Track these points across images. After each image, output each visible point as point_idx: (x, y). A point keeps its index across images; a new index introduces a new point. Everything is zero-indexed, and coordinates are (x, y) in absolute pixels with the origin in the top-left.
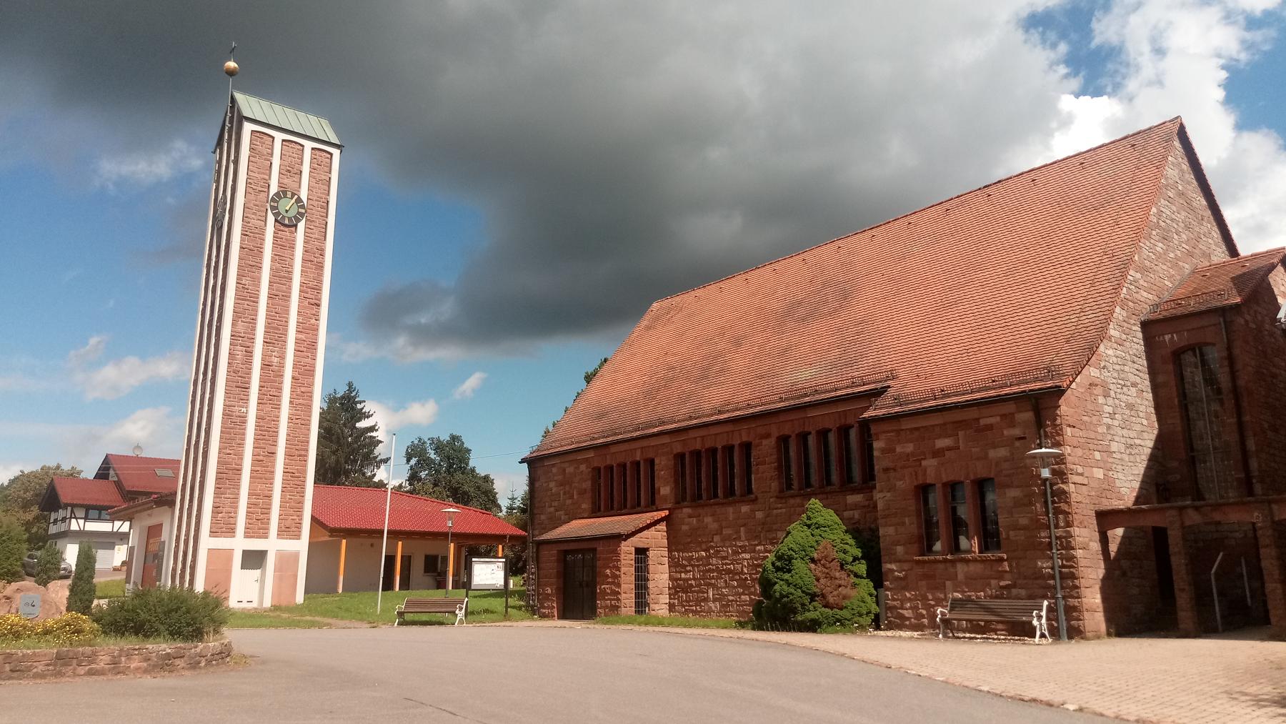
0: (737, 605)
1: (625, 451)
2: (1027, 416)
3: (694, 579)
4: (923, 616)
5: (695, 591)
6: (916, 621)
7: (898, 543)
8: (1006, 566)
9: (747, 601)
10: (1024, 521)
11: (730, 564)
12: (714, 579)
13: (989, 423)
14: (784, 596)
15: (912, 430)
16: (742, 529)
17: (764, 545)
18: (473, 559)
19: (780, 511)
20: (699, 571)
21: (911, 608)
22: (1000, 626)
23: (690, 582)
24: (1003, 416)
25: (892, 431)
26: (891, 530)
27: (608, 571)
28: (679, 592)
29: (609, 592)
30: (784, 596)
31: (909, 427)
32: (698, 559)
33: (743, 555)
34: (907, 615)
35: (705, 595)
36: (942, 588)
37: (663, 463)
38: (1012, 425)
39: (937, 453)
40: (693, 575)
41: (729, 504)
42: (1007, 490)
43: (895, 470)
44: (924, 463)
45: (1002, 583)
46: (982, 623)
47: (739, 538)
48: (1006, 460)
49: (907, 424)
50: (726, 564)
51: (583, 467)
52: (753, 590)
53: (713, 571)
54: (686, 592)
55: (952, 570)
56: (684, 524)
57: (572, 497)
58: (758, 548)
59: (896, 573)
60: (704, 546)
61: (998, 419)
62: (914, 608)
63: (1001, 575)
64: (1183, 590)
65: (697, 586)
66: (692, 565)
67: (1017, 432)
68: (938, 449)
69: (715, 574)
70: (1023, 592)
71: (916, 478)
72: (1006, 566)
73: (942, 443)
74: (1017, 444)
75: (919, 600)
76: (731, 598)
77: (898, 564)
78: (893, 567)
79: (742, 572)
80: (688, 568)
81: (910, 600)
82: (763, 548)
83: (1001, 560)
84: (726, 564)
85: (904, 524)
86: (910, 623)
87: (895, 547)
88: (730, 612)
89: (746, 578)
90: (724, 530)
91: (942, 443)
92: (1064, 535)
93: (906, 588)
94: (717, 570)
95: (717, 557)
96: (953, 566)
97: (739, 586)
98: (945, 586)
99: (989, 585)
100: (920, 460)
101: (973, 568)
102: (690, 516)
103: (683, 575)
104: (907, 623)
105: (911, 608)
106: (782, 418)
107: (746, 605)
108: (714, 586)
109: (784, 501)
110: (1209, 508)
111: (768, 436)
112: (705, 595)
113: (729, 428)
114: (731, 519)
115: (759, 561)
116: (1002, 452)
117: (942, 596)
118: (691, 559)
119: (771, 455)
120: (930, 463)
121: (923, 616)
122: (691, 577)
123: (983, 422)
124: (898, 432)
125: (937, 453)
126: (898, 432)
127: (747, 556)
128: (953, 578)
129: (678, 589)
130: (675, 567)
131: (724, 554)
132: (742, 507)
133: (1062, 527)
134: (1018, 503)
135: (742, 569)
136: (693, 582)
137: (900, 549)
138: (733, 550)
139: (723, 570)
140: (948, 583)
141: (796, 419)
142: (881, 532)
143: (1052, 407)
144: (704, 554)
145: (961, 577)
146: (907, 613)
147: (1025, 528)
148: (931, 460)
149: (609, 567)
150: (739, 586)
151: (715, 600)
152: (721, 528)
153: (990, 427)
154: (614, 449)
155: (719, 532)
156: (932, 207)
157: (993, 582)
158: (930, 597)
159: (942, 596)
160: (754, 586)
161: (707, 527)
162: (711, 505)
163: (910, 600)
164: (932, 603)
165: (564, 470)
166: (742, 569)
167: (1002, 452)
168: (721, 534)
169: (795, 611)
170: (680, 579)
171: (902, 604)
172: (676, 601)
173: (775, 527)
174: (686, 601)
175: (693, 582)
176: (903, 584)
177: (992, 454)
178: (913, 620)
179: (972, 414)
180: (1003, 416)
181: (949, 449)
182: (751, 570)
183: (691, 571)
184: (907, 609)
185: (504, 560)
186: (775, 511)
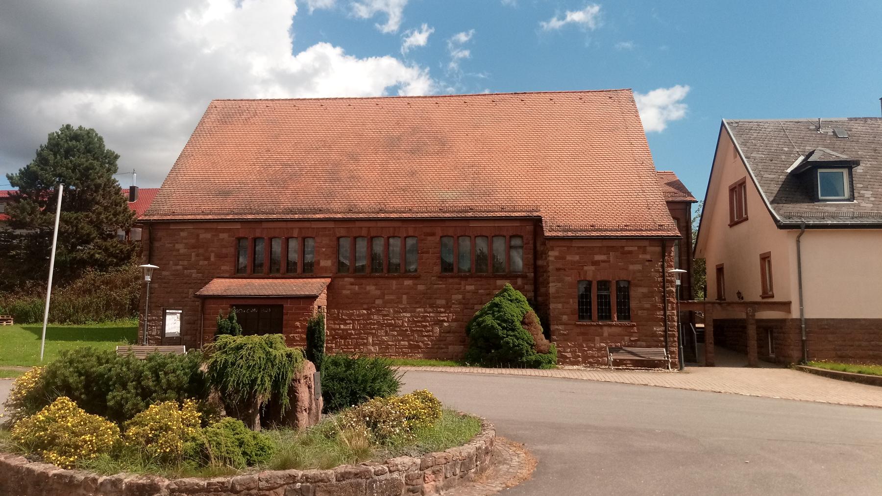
0: (396, 348)
1: (280, 228)
2: (658, 249)
3: (354, 329)
4: (579, 356)
5: (354, 338)
6: (574, 360)
7: (564, 314)
8: (635, 329)
9: (406, 345)
10: (647, 306)
11: (391, 320)
12: (375, 330)
13: (631, 250)
14: (516, 346)
15: (579, 248)
16: (404, 296)
17: (424, 308)
18: (167, 311)
19: (441, 286)
20: (360, 324)
21: (570, 352)
22: (629, 362)
23: (349, 332)
24: (639, 247)
25: (565, 247)
26: (560, 306)
27: (298, 324)
28: (337, 338)
29: (298, 339)
30: (516, 346)
31: (577, 245)
32: (358, 316)
33: (405, 314)
34: (568, 356)
35: (365, 341)
36: (593, 341)
37: (324, 242)
38: (645, 252)
39: (595, 263)
40: (353, 326)
41: (394, 278)
42: (639, 288)
43: (565, 270)
44: (586, 268)
45: (632, 339)
46: (618, 361)
47: (401, 302)
48: (639, 271)
49: (576, 244)
50: (387, 320)
51: (224, 236)
52: (412, 338)
53: (374, 324)
54: (345, 339)
55: (600, 330)
56: (344, 290)
57: (208, 259)
58: (418, 310)
59: (562, 332)
60: (365, 306)
61: (636, 248)
62: (573, 352)
63: (631, 334)
64: (711, 343)
65: (356, 334)
66: (352, 320)
67: (648, 257)
68: (596, 261)
69: (376, 326)
70: (644, 344)
71: (580, 276)
72: (635, 329)
73: (598, 258)
74: (647, 263)
75: (576, 347)
76: (391, 343)
77: (563, 326)
78: (560, 327)
79: (403, 326)
80: (348, 322)
81: (570, 347)
82: (423, 310)
83: (634, 326)
84: (387, 320)
85: (568, 303)
86: (570, 360)
87: (561, 316)
88: (389, 352)
89: (407, 330)
90: (386, 296)
91: (598, 258)
92: (670, 314)
93: (567, 340)
94: (378, 323)
95: (378, 314)
96: (601, 328)
97: (398, 335)
98: (595, 340)
99: (624, 339)
100: (583, 266)
101: (614, 330)
102: (352, 284)
103: (342, 327)
104: (568, 360)
105: (570, 352)
106: (448, 224)
107: (405, 348)
108: (373, 335)
109: (445, 279)
110: (726, 304)
111: (433, 234)
112: (365, 341)
113: (398, 224)
114: (394, 288)
115: (419, 319)
116: (638, 267)
117: (593, 345)
118: (352, 314)
119: (435, 248)
120: (590, 269)
121: (579, 356)
122: (351, 328)
123: (626, 249)
124: (569, 248)
125: (595, 263)
126: (569, 248)
127: (409, 315)
128: (600, 335)
129: (36, 321)
130: (334, 320)
131: (385, 313)
132: (405, 281)
133: (669, 310)
134: (645, 296)
135: (403, 323)
136: (353, 332)
137: (565, 317)
138: (394, 311)
139: (385, 324)
140: (597, 338)
141: (459, 226)
142: (552, 306)
143: (670, 246)
144: (365, 312)
145: (606, 334)
146: (569, 355)
147: (647, 309)
148: (591, 267)
149: (299, 321)
150: (398, 335)
151: (374, 345)
152: (383, 295)
153: (630, 252)
154: (265, 225)
155: (382, 297)
156: (478, 95)
157: (626, 338)
158: (585, 346)
159: (593, 345)
160: (413, 335)
161: (369, 293)
162: (374, 277)
163: (570, 347)
164: (586, 349)
165: (198, 236)
166: (403, 323)
167: (638, 267)
168: (383, 298)
169: (522, 355)
170: (340, 329)
171: (564, 349)
172: (334, 345)
173: (435, 296)
174: (345, 345)
175: (353, 332)
176: (566, 338)
177: (631, 267)
178: (572, 359)
179: (623, 243)
180: (639, 247)
181: (603, 261)
182: (411, 325)
183: (351, 324)
184: (568, 352)
185: (181, 311)
186: (435, 286)
